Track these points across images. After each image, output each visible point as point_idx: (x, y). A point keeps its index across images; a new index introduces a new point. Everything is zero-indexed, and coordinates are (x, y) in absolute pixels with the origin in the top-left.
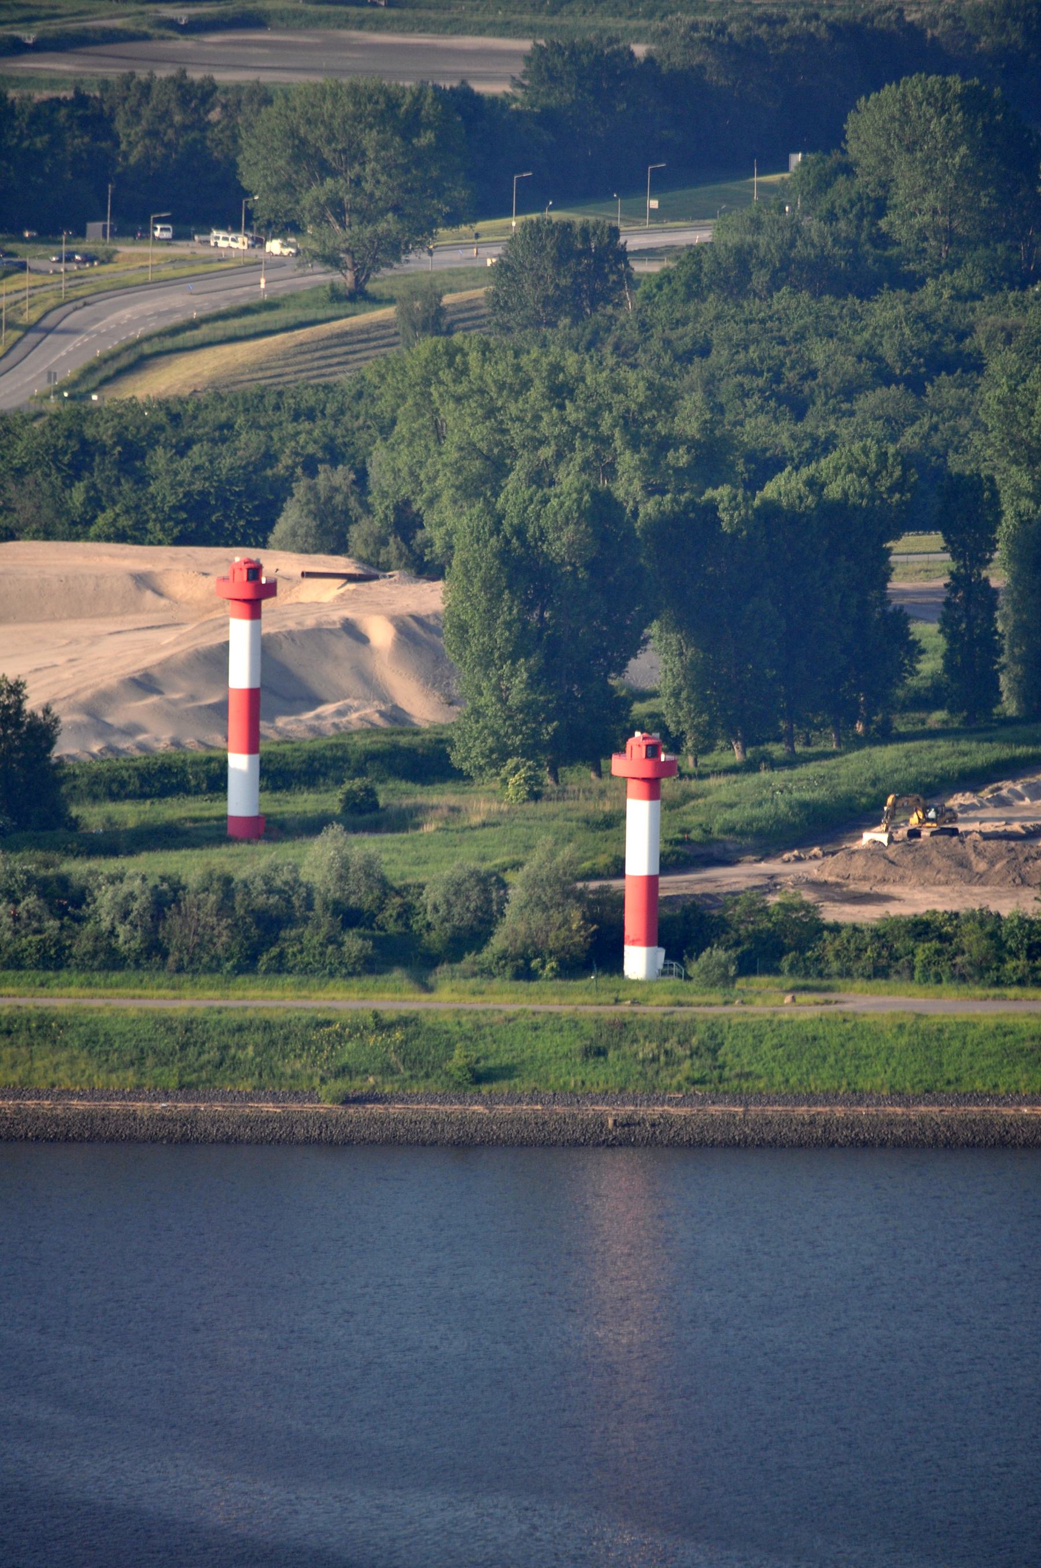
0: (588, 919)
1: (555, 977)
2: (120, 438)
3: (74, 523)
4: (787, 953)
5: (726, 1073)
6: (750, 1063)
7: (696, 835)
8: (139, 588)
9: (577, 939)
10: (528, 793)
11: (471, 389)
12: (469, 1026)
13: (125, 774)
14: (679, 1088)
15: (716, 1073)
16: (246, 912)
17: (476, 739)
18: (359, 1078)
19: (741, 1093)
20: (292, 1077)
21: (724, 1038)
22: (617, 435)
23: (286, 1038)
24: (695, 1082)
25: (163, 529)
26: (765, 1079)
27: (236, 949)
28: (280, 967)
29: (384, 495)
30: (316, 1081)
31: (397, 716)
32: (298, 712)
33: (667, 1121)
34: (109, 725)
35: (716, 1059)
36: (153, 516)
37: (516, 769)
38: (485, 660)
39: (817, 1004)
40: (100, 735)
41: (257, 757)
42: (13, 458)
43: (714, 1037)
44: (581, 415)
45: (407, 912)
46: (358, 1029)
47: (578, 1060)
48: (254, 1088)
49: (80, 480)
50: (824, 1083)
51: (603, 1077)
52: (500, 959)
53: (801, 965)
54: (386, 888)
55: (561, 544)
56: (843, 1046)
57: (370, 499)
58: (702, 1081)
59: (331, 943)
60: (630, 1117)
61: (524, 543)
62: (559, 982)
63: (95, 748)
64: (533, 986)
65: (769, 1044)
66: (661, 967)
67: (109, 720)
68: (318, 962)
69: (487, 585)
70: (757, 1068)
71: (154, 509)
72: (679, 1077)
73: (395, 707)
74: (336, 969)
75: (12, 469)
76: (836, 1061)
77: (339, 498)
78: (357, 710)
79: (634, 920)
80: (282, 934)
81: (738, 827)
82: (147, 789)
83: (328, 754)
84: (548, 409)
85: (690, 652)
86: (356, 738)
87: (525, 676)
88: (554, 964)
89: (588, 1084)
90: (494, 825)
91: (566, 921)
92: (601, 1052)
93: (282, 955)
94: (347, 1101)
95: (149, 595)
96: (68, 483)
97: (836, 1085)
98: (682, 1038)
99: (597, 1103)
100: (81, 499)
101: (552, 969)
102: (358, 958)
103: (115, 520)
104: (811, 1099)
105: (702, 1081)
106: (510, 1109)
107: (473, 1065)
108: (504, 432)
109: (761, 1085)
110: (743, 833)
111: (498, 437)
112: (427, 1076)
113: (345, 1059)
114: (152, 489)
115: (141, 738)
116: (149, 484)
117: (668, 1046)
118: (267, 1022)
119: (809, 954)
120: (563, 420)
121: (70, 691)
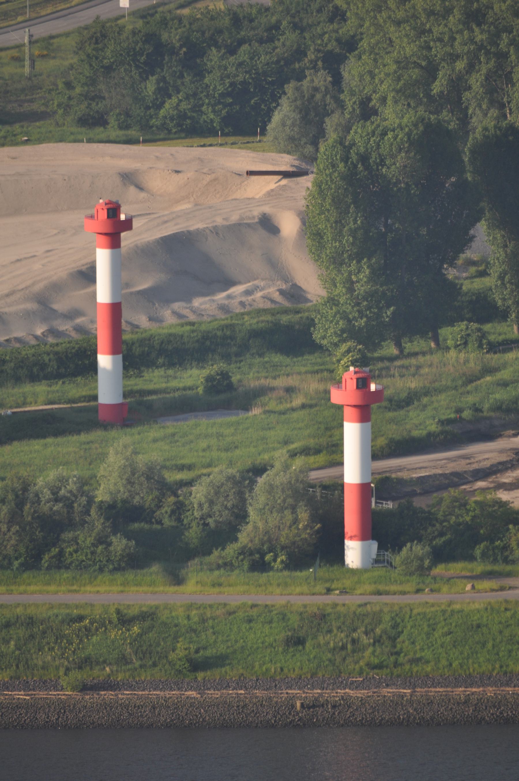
0: (314, 518)
2: (186, 42)
3: (148, 108)
4: (480, 543)
5: (401, 659)
6: (422, 649)
7: (466, 414)
8: (125, 184)
9: (303, 536)
11: (407, 16)
12: (196, 619)
13: (46, 358)
14: (361, 673)
15: (392, 659)
16: (33, 518)
17: (331, 322)
18: (98, 668)
19: (411, 676)
20: (43, 668)
21: (405, 627)
22: (512, 51)
23: (44, 632)
24: (375, 667)
25: (214, 111)
26: (432, 663)
27: (22, 550)
28: (60, 563)
29: (352, 93)
30: (62, 672)
31: (295, 294)
32: (212, 293)
33: (347, 702)
34: (55, 311)
35: (395, 647)
36: (207, 101)
37: (348, 351)
38: (337, 261)
39: (493, 590)
40: (45, 319)
41: (120, 357)
42: (104, 58)
43: (395, 626)
44: (484, 37)
45: (180, 508)
46: (103, 624)
47: (280, 649)
48: (11, 678)
49: (153, 75)
50: (480, 666)
51: (298, 664)
52: (240, 554)
53: (491, 553)
54: (167, 489)
55: (396, 167)
56: (501, 632)
57: (342, 97)
58: (380, 666)
59: (101, 543)
60: (316, 699)
61: (367, 167)
62: (286, 573)
63: (39, 331)
64: (263, 577)
65: (441, 631)
66: (374, 557)
67: (55, 306)
68: (90, 560)
69: (337, 202)
70: (427, 654)
71: (207, 96)
72: (362, 663)
73: (295, 286)
74: (105, 566)
75: (102, 67)
76: (494, 646)
77: (318, 96)
78: (262, 289)
79: (351, 520)
80: (63, 536)
81: (504, 407)
82: (62, 370)
83: (219, 333)
84: (460, 32)
85: (511, 246)
86: (246, 318)
87: (367, 272)
88: (284, 558)
89: (286, 670)
90: (311, 406)
91: (296, 521)
92: (300, 642)
93: (61, 553)
94: (85, 688)
95: (132, 189)
96: (144, 77)
97: (490, 667)
98: (369, 627)
99: (291, 688)
100: (153, 89)
103: (178, 105)
104: (469, 680)
105: (380, 666)
106: (217, 694)
107: (194, 656)
108: (430, 48)
109: (429, 669)
110: (508, 411)
111: (424, 52)
112: (155, 665)
113: (90, 650)
114: (206, 81)
115: (79, 321)
116: (205, 77)
117: (355, 635)
118: (31, 618)
119: (497, 543)
120: (472, 41)
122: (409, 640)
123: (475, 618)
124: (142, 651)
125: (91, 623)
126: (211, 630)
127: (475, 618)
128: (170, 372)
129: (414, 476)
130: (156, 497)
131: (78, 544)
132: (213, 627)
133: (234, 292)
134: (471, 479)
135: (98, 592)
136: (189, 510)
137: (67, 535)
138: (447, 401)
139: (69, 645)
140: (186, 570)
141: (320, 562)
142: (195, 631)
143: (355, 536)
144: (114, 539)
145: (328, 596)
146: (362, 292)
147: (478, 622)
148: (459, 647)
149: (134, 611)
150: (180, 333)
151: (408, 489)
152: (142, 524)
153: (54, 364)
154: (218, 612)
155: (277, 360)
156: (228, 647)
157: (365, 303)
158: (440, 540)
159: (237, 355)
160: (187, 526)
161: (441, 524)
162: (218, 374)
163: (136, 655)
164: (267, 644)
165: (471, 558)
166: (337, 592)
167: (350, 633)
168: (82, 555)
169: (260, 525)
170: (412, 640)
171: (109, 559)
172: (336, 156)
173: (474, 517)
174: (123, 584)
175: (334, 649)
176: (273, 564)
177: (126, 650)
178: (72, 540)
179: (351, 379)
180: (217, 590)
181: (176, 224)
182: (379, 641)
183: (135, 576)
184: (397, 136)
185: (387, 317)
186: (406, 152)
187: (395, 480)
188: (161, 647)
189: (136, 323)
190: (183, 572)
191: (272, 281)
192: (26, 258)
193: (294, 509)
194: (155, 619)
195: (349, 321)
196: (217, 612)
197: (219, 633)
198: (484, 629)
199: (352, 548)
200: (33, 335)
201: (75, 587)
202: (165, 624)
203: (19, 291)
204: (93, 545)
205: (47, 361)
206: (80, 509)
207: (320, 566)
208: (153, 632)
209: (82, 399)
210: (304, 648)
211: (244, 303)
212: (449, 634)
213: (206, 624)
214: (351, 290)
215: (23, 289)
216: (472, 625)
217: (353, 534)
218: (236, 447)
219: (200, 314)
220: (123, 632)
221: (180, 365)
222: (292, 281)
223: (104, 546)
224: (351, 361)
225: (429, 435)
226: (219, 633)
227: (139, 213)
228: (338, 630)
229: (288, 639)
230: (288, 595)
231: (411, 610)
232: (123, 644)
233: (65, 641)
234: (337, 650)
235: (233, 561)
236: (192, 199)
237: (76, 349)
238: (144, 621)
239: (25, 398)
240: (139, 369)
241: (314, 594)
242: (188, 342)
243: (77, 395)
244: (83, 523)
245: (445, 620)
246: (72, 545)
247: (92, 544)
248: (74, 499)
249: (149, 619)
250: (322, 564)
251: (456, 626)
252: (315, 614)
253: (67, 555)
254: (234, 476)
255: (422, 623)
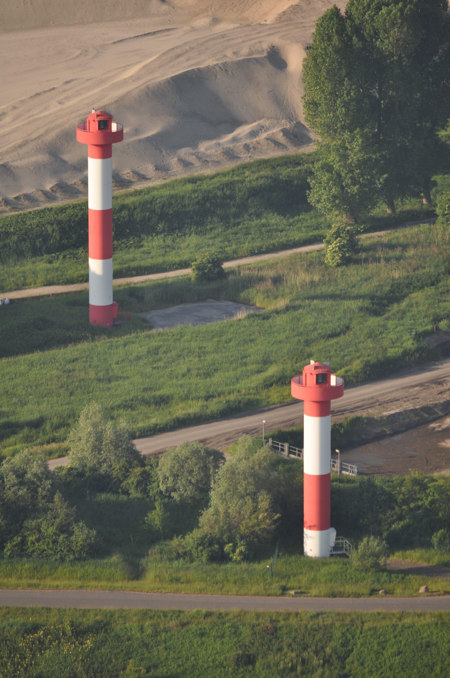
1: (243, 560)
4: (438, 531)
9: (262, 526)
10: (341, 258)
13: (50, 229)
21: (355, 644)
28: (22, 551)
34: (65, 162)
35: (344, 668)
40: (55, 173)
45: (146, 479)
52: (199, 545)
59: (63, 532)
61: (361, 38)
62: (244, 565)
66: (333, 545)
67: (66, 157)
68: (51, 549)
78: (267, 129)
80: (26, 524)
82: (65, 241)
83: (219, 193)
88: (243, 548)
92: (250, 660)
93: (24, 542)
101: (241, 552)
102: (83, 546)
117: (305, 655)
121: (41, 131)
122: (358, 660)
123: (425, 634)
124: (93, 669)
125: (45, 635)
126: (163, 645)
127: (425, 634)
128: (169, 241)
129: (385, 413)
130: (123, 466)
131: (40, 531)
132: (165, 642)
133: (239, 134)
134: (441, 414)
135: (57, 586)
136: (155, 482)
137: (31, 523)
138: (426, 306)
139: (22, 660)
140: (146, 559)
141: (279, 552)
142: (146, 645)
143: (314, 526)
144: (76, 529)
145: (283, 598)
146: (355, 161)
147: (428, 639)
148: (407, 670)
149: (89, 620)
150: (182, 194)
151: (377, 430)
152: (109, 495)
153: (57, 235)
154: (172, 623)
155: (273, 221)
156: (179, 666)
157: (358, 171)
158: (398, 524)
159: (236, 216)
160: (153, 499)
161: (400, 507)
162: (209, 262)
163: (87, 674)
164: (217, 663)
165: (428, 545)
166: (292, 592)
167: (300, 652)
168: (44, 544)
169: (221, 509)
170: (361, 661)
171: (70, 548)
172: (332, 29)
173: (432, 502)
174: (82, 578)
175: (284, 670)
176: (231, 555)
177: (77, 668)
178: (35, 528)
179: (311, 374)
180: (175, 586)
181: (188, 59)
182: (328, 661)
183: (95, 568)
184: (391, 11)
185: (380, 183)
186: (399, 28)
187: (365, 421)
188: (112, 664)
189: (143, 173)
190: (143, 561)
191: (277, 119)
192: (45, 92)
193: (254, 496)
194: (109, 631)
195: (342, 188)
196: (170, 622)
197: (170, 649)
198: (434, 650)
199: (311, 537)
200: (42, 191)
201: (35, 581)
202: (117, 637)
203: (32, 140)
204: (55, 534)
205: (50, 231)
206: (44, 493)
207: (278, 556)
208: (106, 647)
209: (80, 279)
210: (254, 667)
211: (248, 145)
212: (398, 654)
213: (159, 637)
214: (344, 157)
215: (35, 139)
216: (421, 644)
217: (312, 524)
218: (216, 370)
219: (205, 161)
220: (75, 646)
221: (180, 229)
222: (296, 119)
223: (65, 535)
224: (339, 246)
225: (405, 353)
226: (170, 649)
227: (160, 28)
228: (288, 649)
229: (238, 658)
230: (244, 595)
231: (363, 623)
232: (75, 661)
233: (18, 656)
234: (287, 671)
235: (193, 552)
236: (210, 13)
237: (79, 217)
238: (98, 633)
239: (25, 278)
240: (139, 236)
241: (269, 595)
242: (189, 205)
243: (75, 275)
244: (46, 510)
245: (395, 637)
246: (35, 533)
247: (54, 533)
248: (39, 483)
249: (103, 631)
250: (280, 554)
251: (405, 645)
252: (267, 627)
253: (29, 543)
254: (200, 451)
255: (372, 640)
